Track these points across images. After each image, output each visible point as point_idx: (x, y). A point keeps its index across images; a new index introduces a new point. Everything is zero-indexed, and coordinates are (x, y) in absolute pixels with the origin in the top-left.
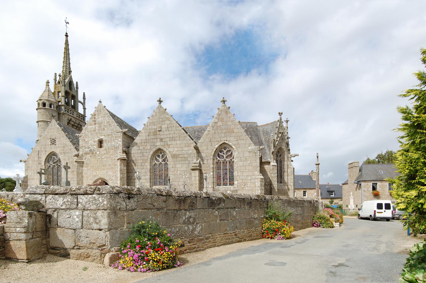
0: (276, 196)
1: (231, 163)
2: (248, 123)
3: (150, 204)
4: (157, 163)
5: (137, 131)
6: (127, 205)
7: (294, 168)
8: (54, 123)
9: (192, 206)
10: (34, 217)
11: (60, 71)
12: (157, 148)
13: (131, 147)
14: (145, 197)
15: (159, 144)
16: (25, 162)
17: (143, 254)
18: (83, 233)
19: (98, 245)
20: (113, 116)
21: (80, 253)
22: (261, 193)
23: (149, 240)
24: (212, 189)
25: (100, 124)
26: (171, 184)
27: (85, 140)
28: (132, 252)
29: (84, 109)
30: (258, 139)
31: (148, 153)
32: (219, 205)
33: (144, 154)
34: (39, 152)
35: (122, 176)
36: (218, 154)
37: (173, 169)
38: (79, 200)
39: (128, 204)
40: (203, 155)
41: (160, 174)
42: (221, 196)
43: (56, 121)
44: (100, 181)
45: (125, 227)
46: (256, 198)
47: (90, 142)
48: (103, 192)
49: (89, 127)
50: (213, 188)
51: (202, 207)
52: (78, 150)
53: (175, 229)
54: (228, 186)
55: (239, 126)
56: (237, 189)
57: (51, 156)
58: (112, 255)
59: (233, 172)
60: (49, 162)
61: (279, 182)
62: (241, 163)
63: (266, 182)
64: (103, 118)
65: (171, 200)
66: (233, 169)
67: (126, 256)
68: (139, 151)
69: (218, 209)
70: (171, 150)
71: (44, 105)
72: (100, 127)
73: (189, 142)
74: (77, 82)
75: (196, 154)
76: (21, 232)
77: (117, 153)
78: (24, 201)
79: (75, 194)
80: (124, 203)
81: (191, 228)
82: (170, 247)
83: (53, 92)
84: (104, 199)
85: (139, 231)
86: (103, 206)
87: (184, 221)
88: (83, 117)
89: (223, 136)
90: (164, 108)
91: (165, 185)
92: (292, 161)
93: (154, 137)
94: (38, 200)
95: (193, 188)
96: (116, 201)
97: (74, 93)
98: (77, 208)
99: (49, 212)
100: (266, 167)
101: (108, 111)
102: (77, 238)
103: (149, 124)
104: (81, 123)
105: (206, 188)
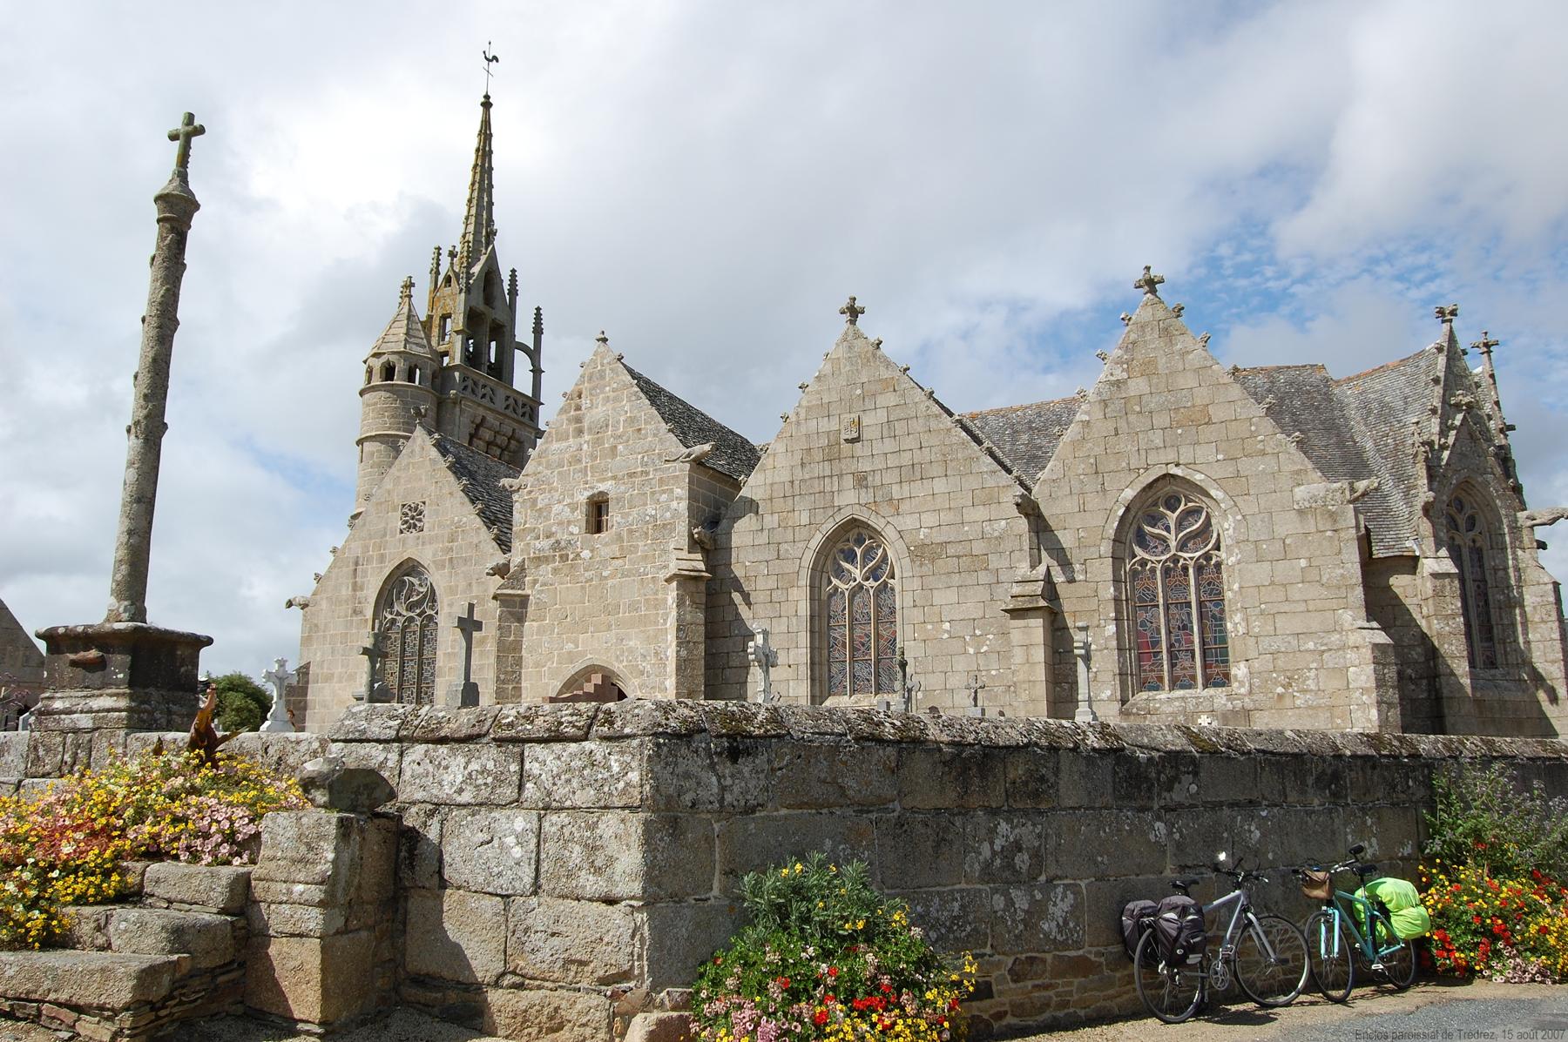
0: (1476, 739)
1: (1209, 571)
2: (1279, 369)
3: (824, 782)
4: (843, 586)
5: (753, 449)
6: (723, 789)
7: (1556, 585)
8: (421, 443)
9: (1036, 795)
10: (356, 837)
11: (453, 232)
12: (841, 518)
13: (724, 523)
14: (804, 750)
15: (850, 502)
16: (304, 606)
17: (802, 1023)
18: (541, 912)
19: (601, 973)
20: (652, 392)
21: (523, 1005)
22: (1384, 722)
23: (826, 955)
24: (1117, 706)
25: (600, 428)
26: (909, 684)
27: (534, 501)
28: (747, 1013)
29: (537, 372)
30: (1341, 444)
31: (802, 545)
32: (1170, 789)
33: (783, 547)
34: (357, 564)
35: (684, 653)
36: (1140, 529)
37: (917, 615)
38: (527, 766)
39: (729, 782)
40: (1066, 539)
41: (850, 637)
42: (1177, 743)
43: (430, 433)
44: (597, 679)
45: (716, 892)
46: (1363, 750)
47: (556, 508)
48: (627, 731)
49: (555, 446)
50: (1124, 701)
51: (1085, 802)
52: (504, 544)
53: (941, 908)
54: (1199, 691)
55: (1236, 391)
56: (1249, 704)
57: (403, 581)
58: (661, 1023)
59: (1220, 619)
60: (392, 606)
61: (1479, 660)
62: (1262, 572)
63: (1403, 662)
64: (610, 406)
65: (921, 764)
66: (1220, 602)
67: (723, 1032)
68: (763, 538)
69: (1168, 809)
70: (908, 522)
71: (389, 372)
72: (598, 442)
73: (990, 483)
74: (513, 271)
75: (1026, 537)
76: (308, 903)
77: (665, 551)
78: (326, 768)
79: (514, 742)
80: (714, 779)
81: (1021, 902)
82: (929, 995)
83: (423, 318)
84: (628, 758)
85: (782, 911)
86: (624, 792)
87: (988, 865)
88: (529, 407)
89: (1158, 442)
90: (873, 339)
91: (879, 690)
92: (1542, 545)
93: (826, 469)
94: (374, 764)
95: (1015, 702)
96: (679, 770)
97: (499, 315)
98: (517, 802)
99: (409, 822)
100: (1399, 583)
101: (631, 371)
102: (513, 937)
103: (802, 416)
104: (524, 433)
105: (1090, 700)
